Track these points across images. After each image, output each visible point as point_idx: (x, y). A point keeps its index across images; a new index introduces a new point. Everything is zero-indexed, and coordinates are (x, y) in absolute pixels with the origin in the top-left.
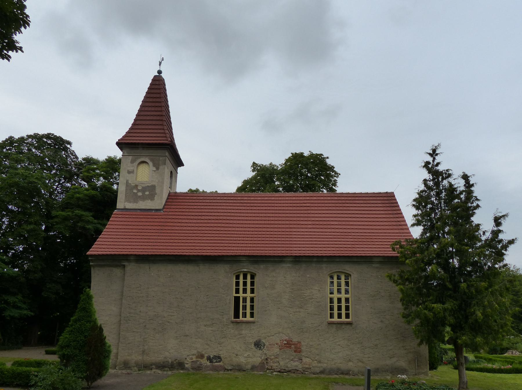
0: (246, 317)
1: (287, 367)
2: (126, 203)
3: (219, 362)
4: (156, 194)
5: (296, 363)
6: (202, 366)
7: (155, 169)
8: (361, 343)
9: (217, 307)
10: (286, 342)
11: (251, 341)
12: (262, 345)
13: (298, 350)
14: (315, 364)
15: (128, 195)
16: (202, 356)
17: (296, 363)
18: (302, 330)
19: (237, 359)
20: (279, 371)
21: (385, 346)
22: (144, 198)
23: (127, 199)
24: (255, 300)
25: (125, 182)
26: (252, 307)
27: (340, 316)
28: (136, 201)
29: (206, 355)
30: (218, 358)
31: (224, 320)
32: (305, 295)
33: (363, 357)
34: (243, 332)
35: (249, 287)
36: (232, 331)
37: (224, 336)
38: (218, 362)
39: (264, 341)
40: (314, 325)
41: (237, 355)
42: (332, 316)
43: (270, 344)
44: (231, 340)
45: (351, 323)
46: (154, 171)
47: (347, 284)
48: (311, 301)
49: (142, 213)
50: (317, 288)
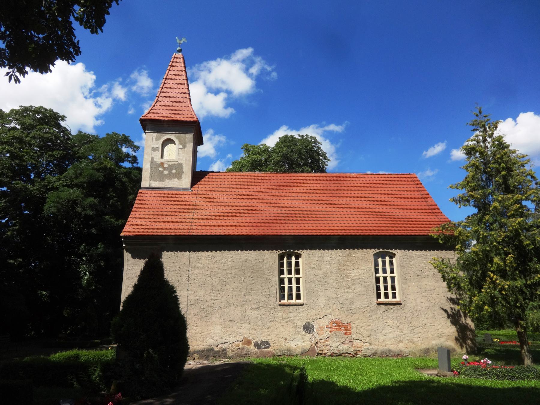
0: (292, 299)
1: (338, 350)
2: (151, 182)
3: (268, 347)
4: (183, 173)
5: (346, 347)
6: (250, 353)
7: (181, 147)
8: (410, 323)
9: (263, 289)
10: (336, 324)
11: (300, 324)
12: (311, 328)
13: (348, 332)
14: (367, 346)
15: (153, 173)
16: (249, 342)
17: (346, 347)
18: (351, 311)
19: (287, 344)
20: (331, 355)
21: (434, 325)
22: (170, 177)
23: (152, 178)
24: (301, 280)
25: (150, 160)
26: (378, 288)
27: (386, 296)
28: (162, 179)
29: (253, 341)
30: (267, 344)
31: (271, 302)
32: (352, 275)
33: (413, 337)
34: (292, 315)
35: (293, 268)
36: (280, 314)
37: (271, 320)
38: (266, 348)
39: (313, 323)
40: (363, 306)
41: (286, 340)
42: (379, 296)
43: (319, 327)
44: (279, 324)
45: (400, 302)
46: (181, 149)
47: (391, 263)
48: (358, 281)
49: (170, 192)
50: (363, 268)
